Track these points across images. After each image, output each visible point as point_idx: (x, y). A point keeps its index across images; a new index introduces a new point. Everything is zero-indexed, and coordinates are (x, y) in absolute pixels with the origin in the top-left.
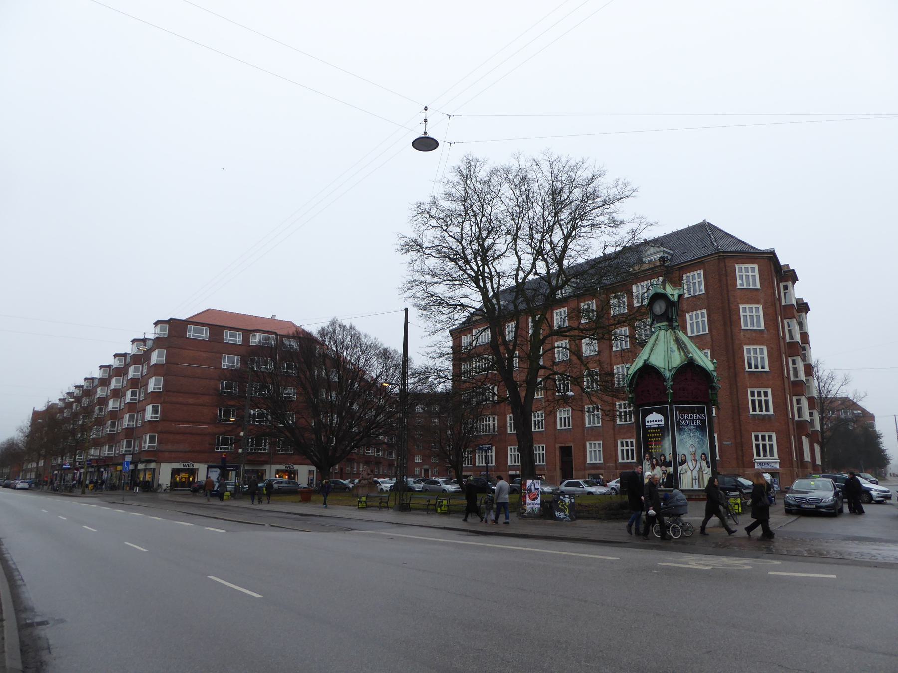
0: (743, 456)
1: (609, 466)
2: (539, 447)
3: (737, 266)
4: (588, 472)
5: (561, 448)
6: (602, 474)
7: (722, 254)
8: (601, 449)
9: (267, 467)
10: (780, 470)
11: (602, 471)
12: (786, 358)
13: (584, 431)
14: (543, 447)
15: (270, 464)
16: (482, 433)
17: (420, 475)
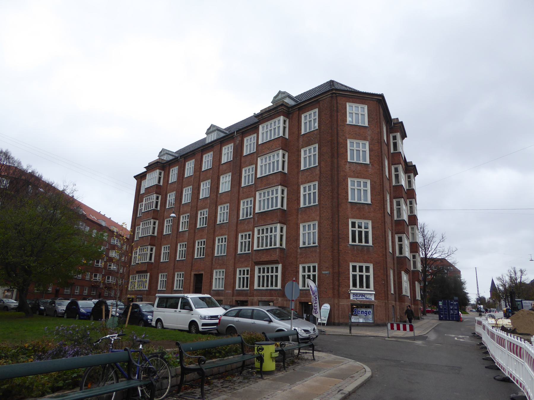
0: (339, 286)
1: (228, 292)
3: (349, 120)
7: (334, 92)
12: (390, 199)
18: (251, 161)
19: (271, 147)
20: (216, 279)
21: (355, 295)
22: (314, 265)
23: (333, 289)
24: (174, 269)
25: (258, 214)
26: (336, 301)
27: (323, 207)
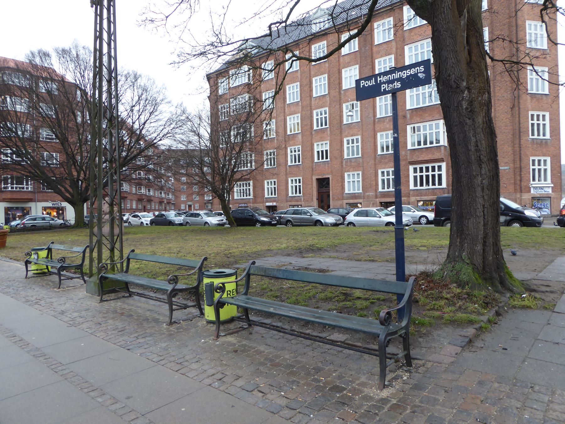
0: (521, 181)
2: (271, 182)
4: (345, 201)
5: (318, 179)
6: (361, 203)
8: (360, 179)
9: (32, 205)
10: (552, 195)
11: (360, 201)
13: (342, 163)
14: (275, 182)
15: (35, 201)
16: (243, 169)
17: (186, 209)
18: (387, 50)
19: (424, 32)
20: (349, 182)
21: (535, 188)
22: (299, 178)
23: (515, 184)
24: (286, 174)
25: (411, 111)
26: (518, 196)
27: (498, 100)
